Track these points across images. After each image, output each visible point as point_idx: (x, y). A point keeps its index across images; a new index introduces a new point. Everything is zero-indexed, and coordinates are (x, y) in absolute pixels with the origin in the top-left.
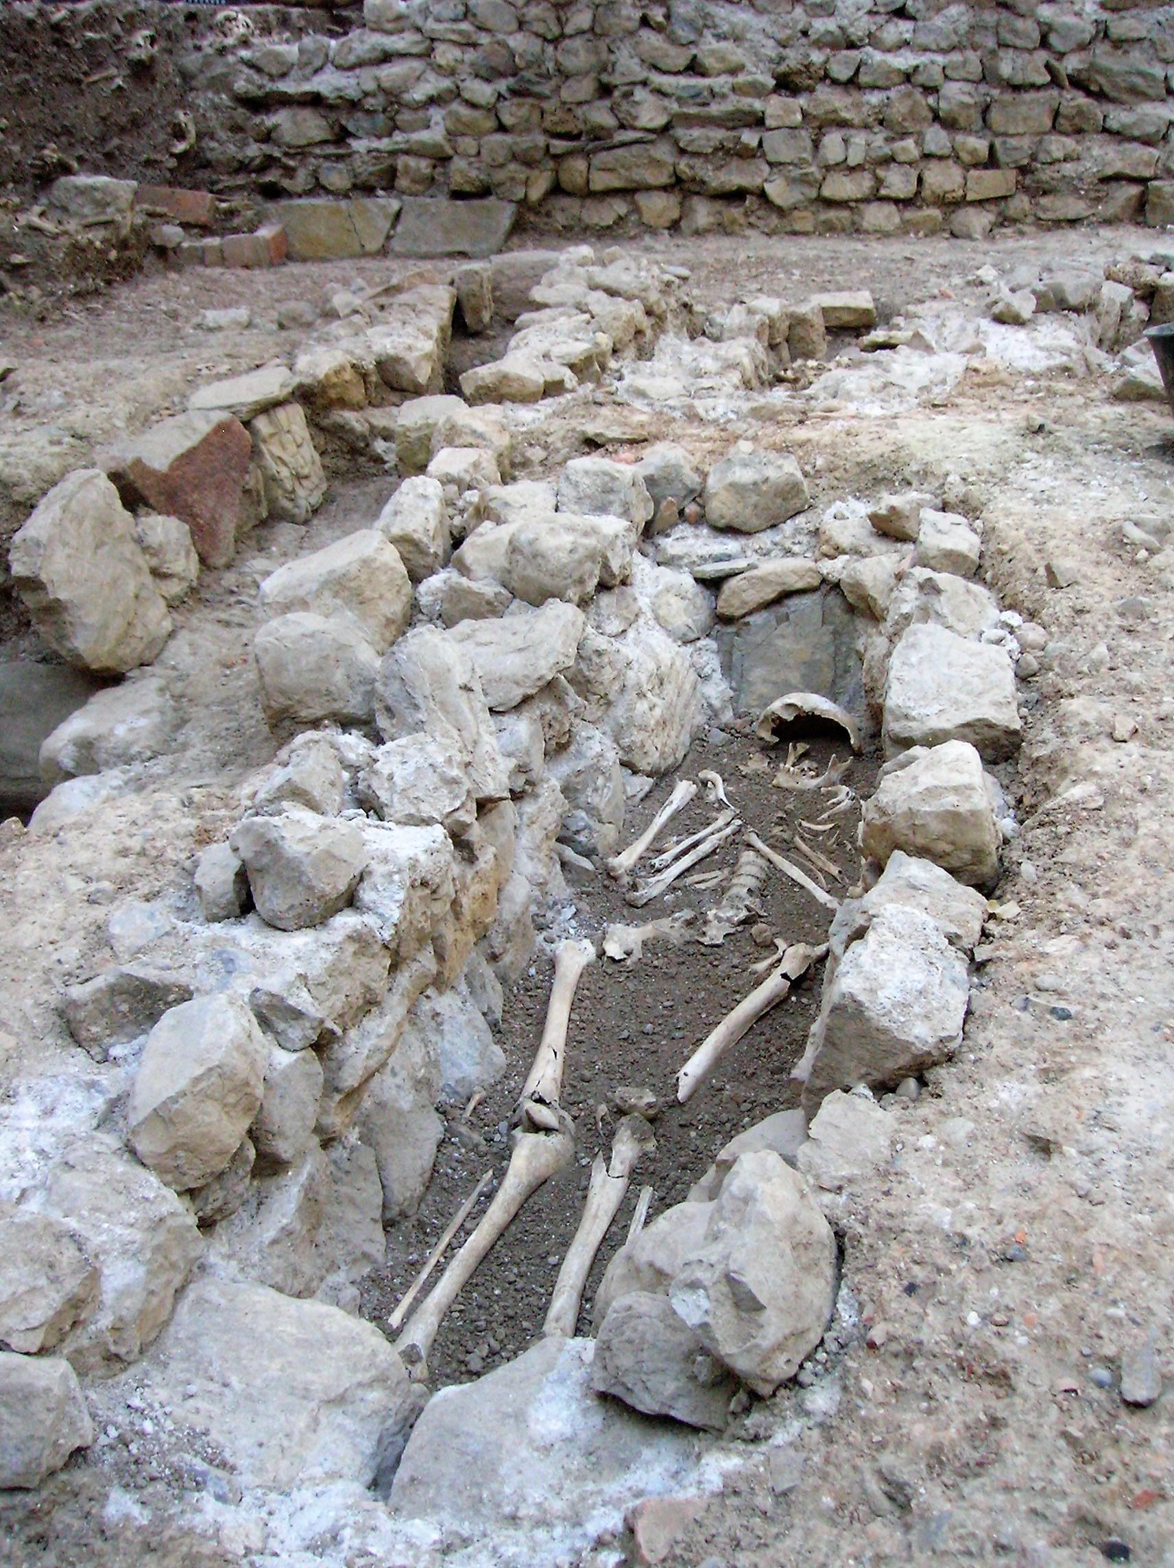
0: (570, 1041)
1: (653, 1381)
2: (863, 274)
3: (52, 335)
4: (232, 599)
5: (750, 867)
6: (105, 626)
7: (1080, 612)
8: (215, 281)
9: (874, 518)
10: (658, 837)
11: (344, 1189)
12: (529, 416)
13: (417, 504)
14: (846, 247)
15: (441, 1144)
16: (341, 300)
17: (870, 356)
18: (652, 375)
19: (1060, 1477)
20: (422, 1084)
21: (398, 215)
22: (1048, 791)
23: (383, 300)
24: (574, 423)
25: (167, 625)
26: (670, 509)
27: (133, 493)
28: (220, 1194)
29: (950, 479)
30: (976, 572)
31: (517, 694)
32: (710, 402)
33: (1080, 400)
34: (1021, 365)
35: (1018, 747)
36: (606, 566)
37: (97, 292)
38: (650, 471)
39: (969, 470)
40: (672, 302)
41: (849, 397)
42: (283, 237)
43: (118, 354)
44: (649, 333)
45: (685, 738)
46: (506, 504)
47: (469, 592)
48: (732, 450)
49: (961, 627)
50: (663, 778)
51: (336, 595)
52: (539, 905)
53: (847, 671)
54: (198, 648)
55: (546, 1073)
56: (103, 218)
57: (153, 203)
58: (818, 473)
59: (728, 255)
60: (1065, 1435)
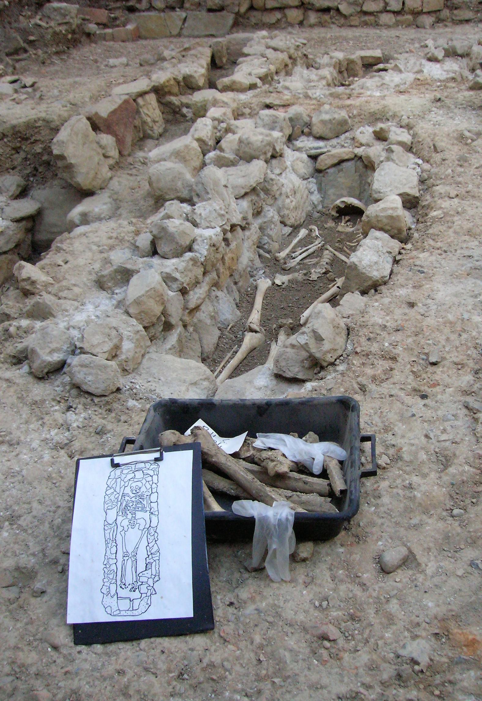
0: (263, 308)
1: (291, 369)
2: (378, 43)
3: (48, 69)
4: (132, 167)
5: (327, 256)
6: (88, 173)
7: (444, 160)
8: (111, 47)
9: (375, 132)
10: (294, 248)
11: (189, 345)
12: (243, 97)
13: (203, 127)
14: (372, 32)
15: (220, 337)
16: (167, 53)
17: (377, 74)
18: (291, 81)
19: (409, 381)
20: (213, 318)
21: (185, 20)
22: (427, 215)
23: (184, 53)
24: (261, 99)
25: (109, 174)
26: (298, 130)
27: (96, 125)
28: (153, 331)
29: (403, 117)
30: (409, 149)
31: (243, 192)
32: (314, 91)
33: (457, 89)
34: (436, 77)
35: (418, 203)
36: (274, 149)
37: (64, 52)
38: (290, 116)
39: (410, 114)
40: (300, 53)
41: (368, 89)
42: (137, 29)
43: (77, 76)
44: (290, 66)
45: (304, 215)
46: (237, 127)
47: (225, 157)
48: (322, 108)
50: (296, 228)
51: (176, 158)
52: (251, 267)
53: (365, 190)
54: (121, 183)
55: (255, 317)
56: (65, 21)
57: (83, 14)
58: (355, 117)
59: (323, 35)
60: (412, 371)
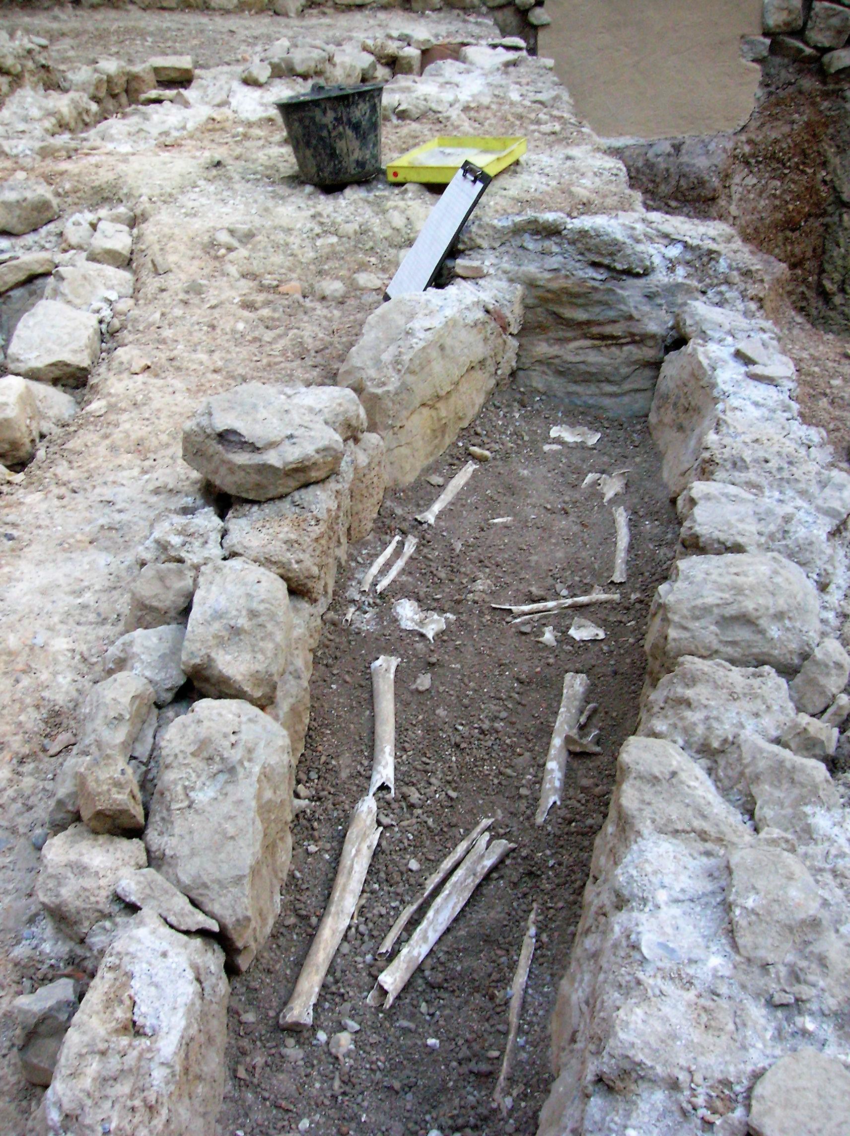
7: (163, 290)
41: (112, 139)
49: (77, 301)
